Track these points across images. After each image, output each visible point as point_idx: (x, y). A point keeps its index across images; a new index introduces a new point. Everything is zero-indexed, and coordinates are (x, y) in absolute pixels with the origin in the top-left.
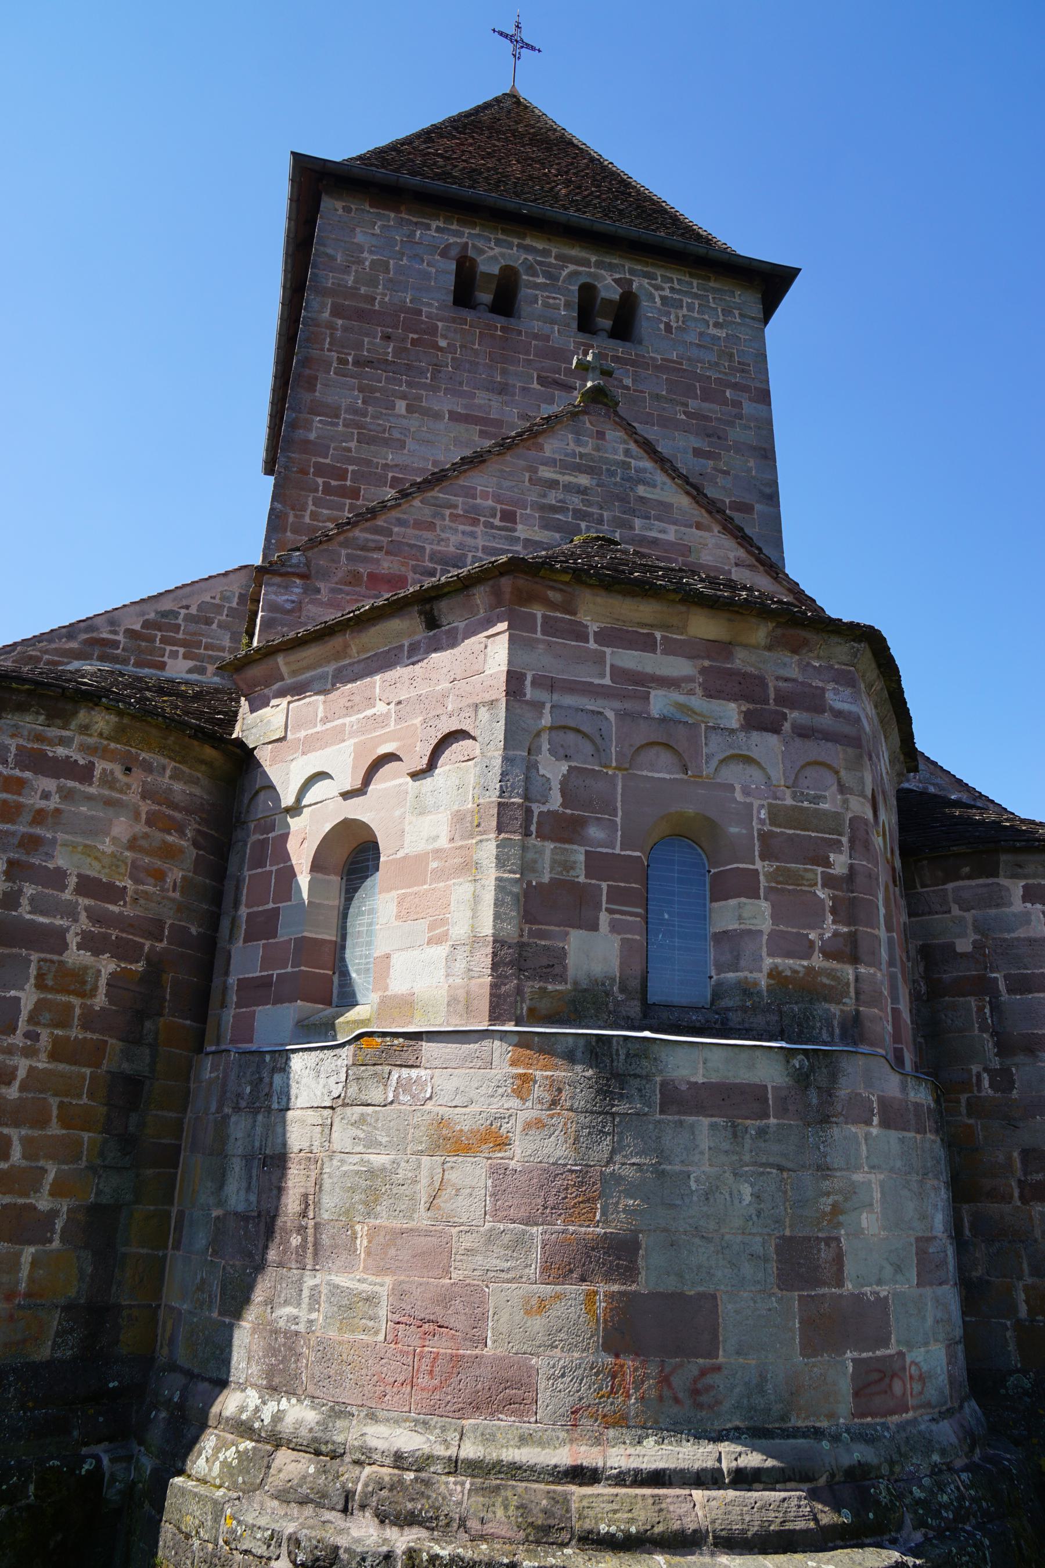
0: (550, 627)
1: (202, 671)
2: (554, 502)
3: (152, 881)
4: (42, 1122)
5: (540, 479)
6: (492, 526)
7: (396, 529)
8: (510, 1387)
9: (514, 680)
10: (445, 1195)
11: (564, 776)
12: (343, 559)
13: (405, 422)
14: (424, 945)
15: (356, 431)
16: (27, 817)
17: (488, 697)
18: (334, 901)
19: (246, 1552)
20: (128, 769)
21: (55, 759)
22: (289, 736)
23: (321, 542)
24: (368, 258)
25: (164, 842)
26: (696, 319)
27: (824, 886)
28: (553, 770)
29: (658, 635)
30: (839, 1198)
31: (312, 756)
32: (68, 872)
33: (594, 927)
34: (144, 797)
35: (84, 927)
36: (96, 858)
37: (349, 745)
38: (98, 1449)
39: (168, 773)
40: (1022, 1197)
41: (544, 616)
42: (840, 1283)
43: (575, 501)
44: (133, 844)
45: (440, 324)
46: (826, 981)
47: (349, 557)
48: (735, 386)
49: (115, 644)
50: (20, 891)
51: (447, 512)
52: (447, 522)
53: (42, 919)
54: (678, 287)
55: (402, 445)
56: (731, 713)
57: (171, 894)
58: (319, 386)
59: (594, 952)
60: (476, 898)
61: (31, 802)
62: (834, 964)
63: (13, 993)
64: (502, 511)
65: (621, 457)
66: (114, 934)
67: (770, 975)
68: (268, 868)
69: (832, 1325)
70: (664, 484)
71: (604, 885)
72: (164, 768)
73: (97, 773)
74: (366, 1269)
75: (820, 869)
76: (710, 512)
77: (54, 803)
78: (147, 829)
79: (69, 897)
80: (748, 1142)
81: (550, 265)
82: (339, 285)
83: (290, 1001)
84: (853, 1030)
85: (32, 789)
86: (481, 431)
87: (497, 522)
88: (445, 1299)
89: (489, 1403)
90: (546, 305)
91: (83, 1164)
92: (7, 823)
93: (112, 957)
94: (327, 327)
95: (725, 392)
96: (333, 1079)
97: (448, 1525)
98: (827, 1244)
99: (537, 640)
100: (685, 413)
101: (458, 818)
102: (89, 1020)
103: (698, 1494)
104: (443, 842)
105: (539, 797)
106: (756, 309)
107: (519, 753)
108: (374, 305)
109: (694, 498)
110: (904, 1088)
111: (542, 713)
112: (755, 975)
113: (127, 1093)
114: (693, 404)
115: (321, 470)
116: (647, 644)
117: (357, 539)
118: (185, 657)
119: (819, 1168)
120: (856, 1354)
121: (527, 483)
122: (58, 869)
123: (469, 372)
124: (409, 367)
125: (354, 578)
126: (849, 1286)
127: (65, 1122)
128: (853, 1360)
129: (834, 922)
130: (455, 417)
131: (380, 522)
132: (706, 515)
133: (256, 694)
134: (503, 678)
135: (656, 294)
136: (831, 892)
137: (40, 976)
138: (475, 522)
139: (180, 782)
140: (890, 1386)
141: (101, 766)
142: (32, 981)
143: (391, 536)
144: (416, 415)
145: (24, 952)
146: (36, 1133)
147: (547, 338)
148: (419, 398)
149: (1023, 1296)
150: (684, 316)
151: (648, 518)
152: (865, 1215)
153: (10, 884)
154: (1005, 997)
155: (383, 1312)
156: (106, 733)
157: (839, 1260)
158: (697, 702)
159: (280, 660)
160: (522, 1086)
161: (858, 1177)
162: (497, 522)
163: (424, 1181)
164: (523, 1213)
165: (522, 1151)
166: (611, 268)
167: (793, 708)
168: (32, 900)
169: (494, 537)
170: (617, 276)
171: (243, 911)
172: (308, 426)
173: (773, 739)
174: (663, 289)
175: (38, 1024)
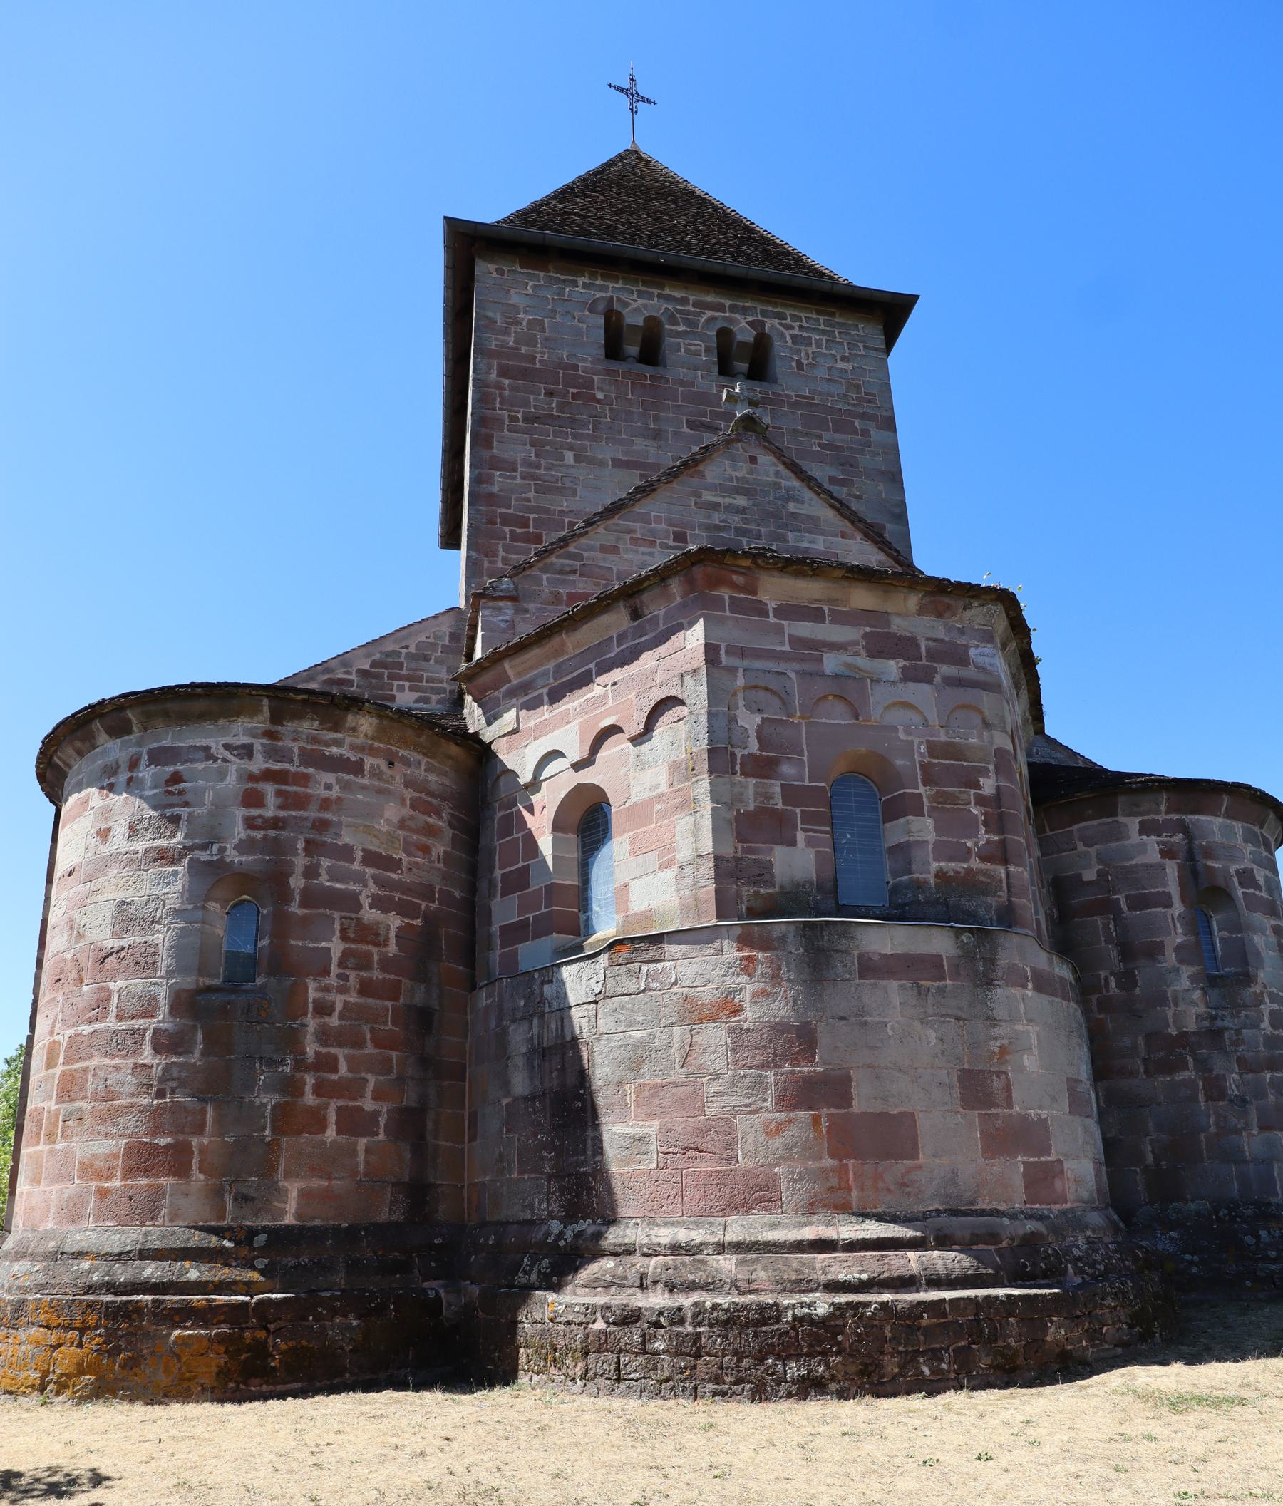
0: (737, 606)
1: (426, 700)
3: (420, 853)
4: (359, 1044)
5: (704, 503)
6: (667, 547)
7: (586, 554)
8: (760, 1190)
9: (711, 651)
10: (694, 1055)
12: (545, 583)
14: (654, 874)
16: (314, 805)
17: (690, 667)
18: (574, 854)
19: (568, 1323)
20: (391, 764)
21: (331, 757)
22: (521, 726)
23: (524, 569)
27: (977, 804)
28: (749, 721)
29: (826, 609)
30: (1005, 1042)
31: (542, 740)
33: (793, 843)
37: (575, 725)
38: (435, 1284)
39: (423, 767)
40: (1146, 1072)
41: (731, 598)
42: (1010, 1106)
43: (736, 520)
44: (402, 824)
45: (595, 377)
46: (982, 878)
48: (864, 416)
49: (350, 682)
50: (318, 865)
51: (628, 536)
53: (338, 886)
54: (806, 325)
55: (575, 493)
56: (892, 668)
57: (437, 865)
59: (796, 861)
60: (696, 826)
62: (987, 866)
63: (323, 944)
65: (771, 478)
66: (397, 896)
67: (937, 876)
69: (1002, 1139)
70: (811, 499)
71: (798, 810)
72: (419, 763)
73: (367, 767)
74: (636, 1118)
75: (972, 791)
76: (852, 522)
77: (336, 792)
78: (412, 813)
80: (930, 1000)
81: (689, 313)
82: (502, 346)
83: (547, 935)
84: (1008, 917)
85: (317, 782)
87: (671, 543)
88: (702, 1131)
89: (744, 1203)
90: (688, 352)
91: (394, 1076)
96: (593, 981)
97: (722, 1286)
98: (998, 1077)
99: (727, 618)
100: (819, 445)
101: (674, 767)
102: (386, 964)
103: (911, 1255)
104: (664, 788)
106: (879, 340)
109: (838, 510)
110: (1051, 963)
112: (924, 876)
113: (422, 1020)
114: (827, 436)
115: (506, 520)
116: (816, 615)
118: (411, 689)
119: (988, 1018)
120: (1025, 1159)
124: (572, 420)
125: (556, 599)
126: (1017, 1108)
127: (377, 1043)
128: (1024, 1163)
129: (986, 832)
130: (618, 463)
131: (571, 549)
132: (849, 524)
134: (702, 649)
135: (787, 333)
136: (982, 808)
137: (343, 931)
138: (652, 543)
139: (431, 772)
140: (1053, 1183)
141: (369, 762)
142: (338, 934)
145: (328, 912)
146: (357, 1052)
147: (692, 384)
148: (584, 448)
149: (1149, 1148)
151: (799, 531)
152: (1026, 1056)
154: (1127, 913)
155: (653, 1147)
156: (370, 734)
157: (1008, 1088)
158: (863, 661)
159: (507, 665)
160: (748, 967)
161: (1019, 1027)
162: (671, 543)
163: (677, 1046)
164: (758, 1060)
165: (751, 1014)
166: (744, 311)
167: (942, 662)
168: (329, 870)
170: (750, 319)
171: (498, 873)
173: (925, 687)
174: (793, 328)
175: (346, 968)
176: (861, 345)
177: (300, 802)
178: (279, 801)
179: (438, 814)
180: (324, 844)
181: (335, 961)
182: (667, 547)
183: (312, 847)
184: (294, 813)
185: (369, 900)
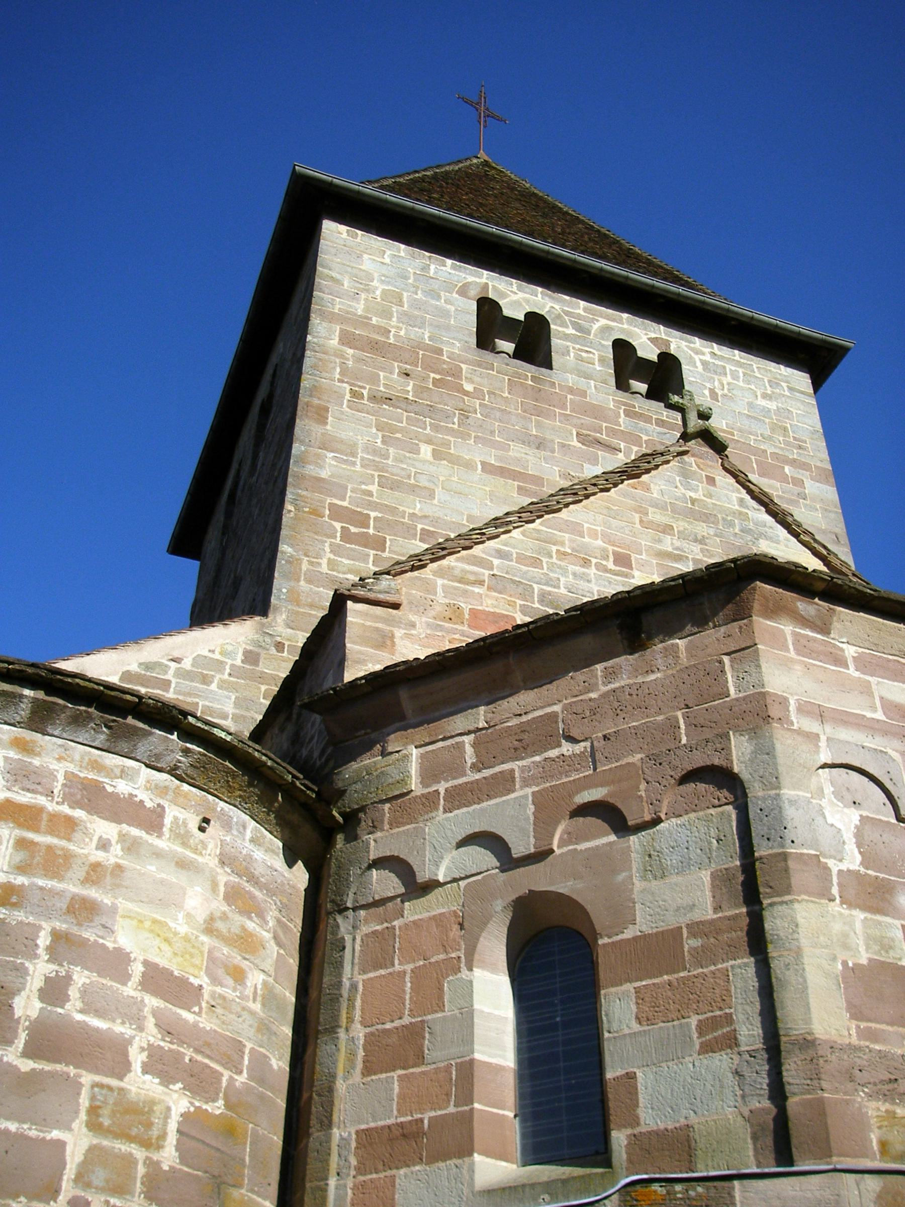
2: (670, 549)
3: (230, 981)
6: (606, 570)
11: (856, 827)
12: (439, 590)
13: (432, 469)
15: (376, 474)
21: (115, 796)
24: (379, 287)
25: (243, 928)
26: (742, 389)
32: (132, 956)
34: (222, 863)
35: (152, 1040)
36: (166, 940)
45: (464, 366)
47: (446, 590)
48: (793, 463)
50: (68, 978)
51: (554, 548)
52: (554, 560)
55: (432, 496)
57: (251, 1005)
58: (330, 419)
61: (85, 851)
63: (55, 1134)
64: (615, 554)
68: (397, 967)
73: (168, 821)
77: (115, 855)
78: (225, 908)
79: (132, 993)
81: (579, 316)
82: (348, 312)
86: (519, 488)
87: (611, 565)
92: (52, 878)
93: (184, 1088)
94: (336, 355)
95: (783, 468)
105: (833, 853)
107: (801, 793)
108: (388, 338)
111: (817, 746)
117: (453, 568)
121: (638, 526)
122: (119, 951)
123: (501, 421)
125: (454, 614)
130: (487, 468)
133: (356, 741)
137: (93, 1111)
141: (172, 813)
142: (83, 1116)
143: (492, 569)
144: (445, 462)
145: (72, 1071)
148: (447, 445)
150: (729, 384)
153: (54, 967)
169: (610, 582)
170: (653, 335)
172: (319, 462)
174: (703, 354)
175: (88, 1185)
176: (784, 385)
177: (56, 863)
178: (20, 857)
179: (261, 915)
180: (84, 943)
181: (70, 1172)
182: (606, 570)
183: (64, 946)
184: (41, 882)
185: (144, 1056)
